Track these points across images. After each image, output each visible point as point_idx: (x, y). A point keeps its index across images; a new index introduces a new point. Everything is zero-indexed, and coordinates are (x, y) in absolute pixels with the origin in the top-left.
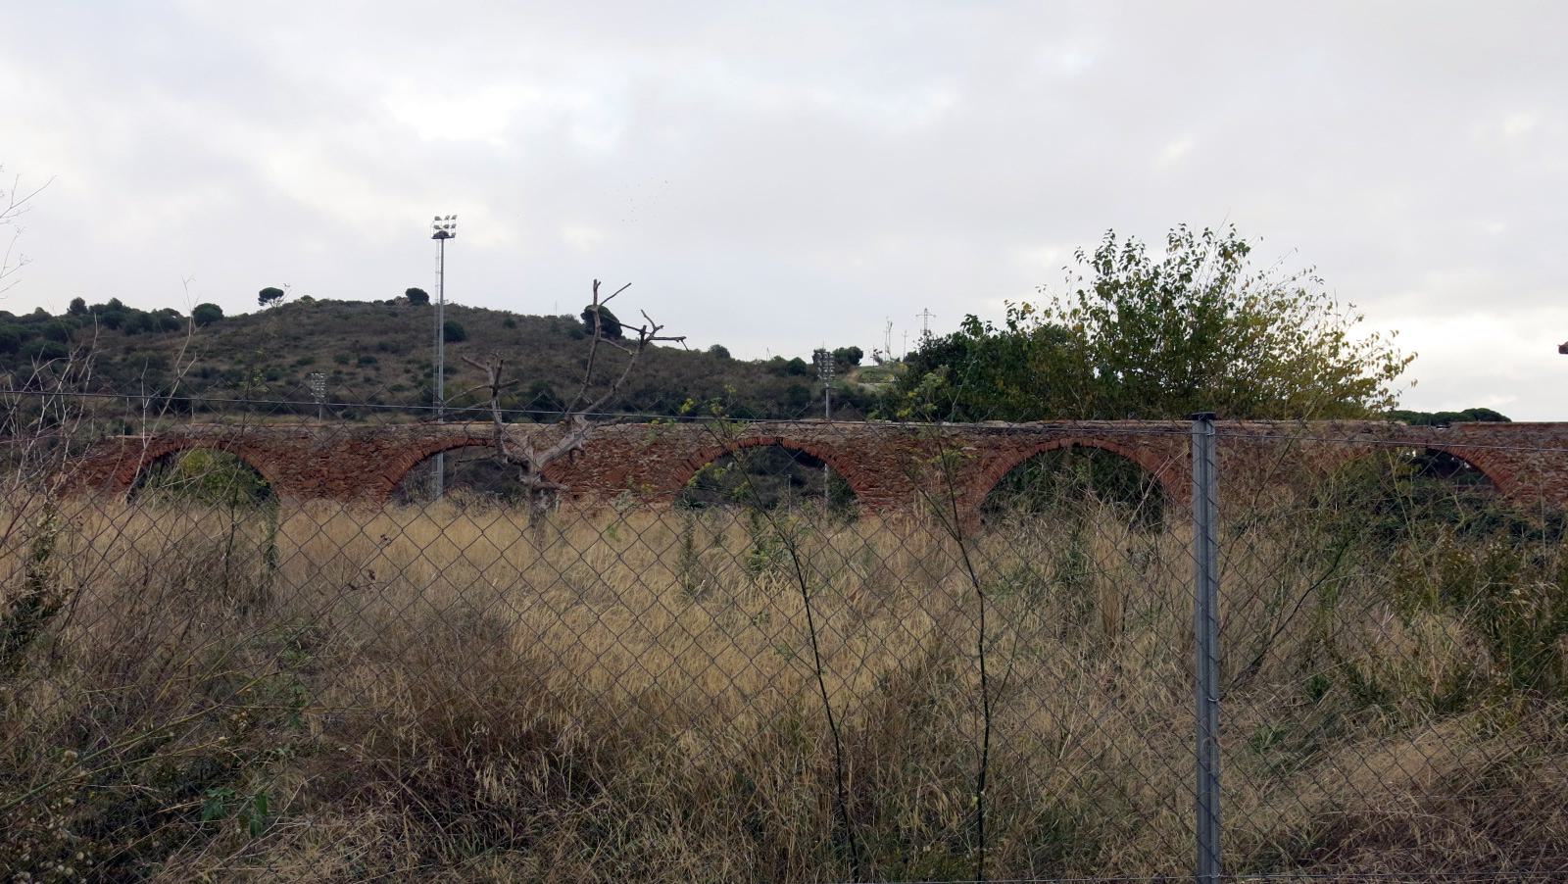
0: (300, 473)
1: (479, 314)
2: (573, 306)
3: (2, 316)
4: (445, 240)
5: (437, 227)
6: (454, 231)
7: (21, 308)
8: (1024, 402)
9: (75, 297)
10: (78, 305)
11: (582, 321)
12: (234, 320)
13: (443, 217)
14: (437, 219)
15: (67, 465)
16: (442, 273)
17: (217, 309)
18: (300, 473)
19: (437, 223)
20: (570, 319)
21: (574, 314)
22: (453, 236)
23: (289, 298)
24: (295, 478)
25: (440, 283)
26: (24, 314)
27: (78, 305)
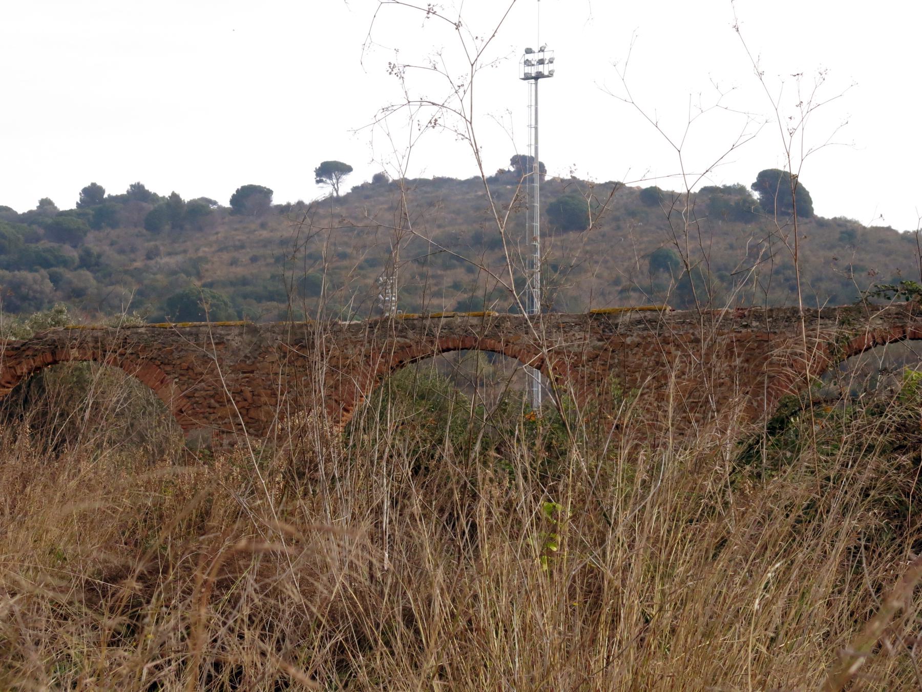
0: (212, 397)
1: (444, 191)
2: (89, 184)
3: (2, 212)
4: (540, 80)
5: (527, 63)
6: (551, 67)
7: (24, 204)
8: (472, 580)
9: (87, 184)
10: (92, 193)
11: (756, 195)
12: (285, 210)
13: (536, 49)
14: (529, 51)
15: (702, 305)
16: (536, 128)
17: (266, 193)
18: (212, 397)
19: (529, 57)
20: (740, 190)
21: (742, 183)
22: (551, 75)
23: (360, 176)
24: (205, 404)
25: (533, 142)
26: (670, 189)
27: (92, 193)
